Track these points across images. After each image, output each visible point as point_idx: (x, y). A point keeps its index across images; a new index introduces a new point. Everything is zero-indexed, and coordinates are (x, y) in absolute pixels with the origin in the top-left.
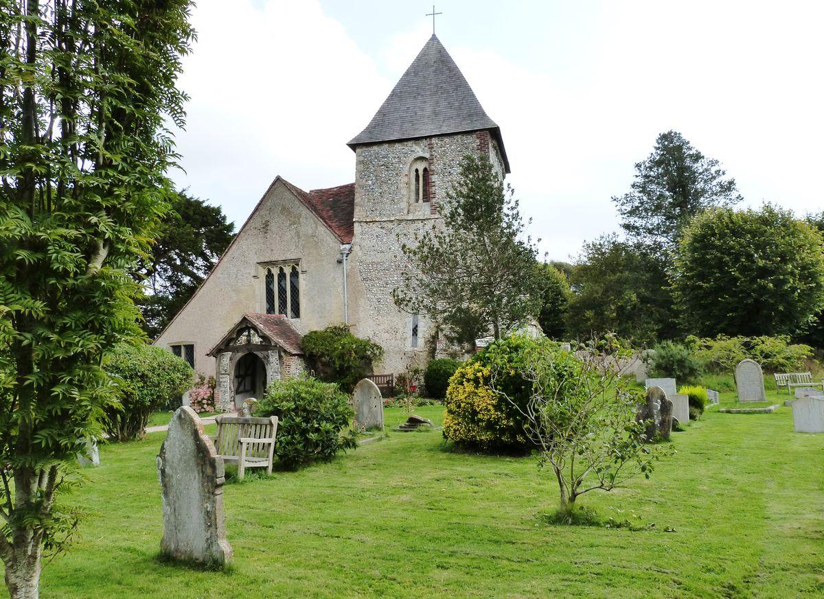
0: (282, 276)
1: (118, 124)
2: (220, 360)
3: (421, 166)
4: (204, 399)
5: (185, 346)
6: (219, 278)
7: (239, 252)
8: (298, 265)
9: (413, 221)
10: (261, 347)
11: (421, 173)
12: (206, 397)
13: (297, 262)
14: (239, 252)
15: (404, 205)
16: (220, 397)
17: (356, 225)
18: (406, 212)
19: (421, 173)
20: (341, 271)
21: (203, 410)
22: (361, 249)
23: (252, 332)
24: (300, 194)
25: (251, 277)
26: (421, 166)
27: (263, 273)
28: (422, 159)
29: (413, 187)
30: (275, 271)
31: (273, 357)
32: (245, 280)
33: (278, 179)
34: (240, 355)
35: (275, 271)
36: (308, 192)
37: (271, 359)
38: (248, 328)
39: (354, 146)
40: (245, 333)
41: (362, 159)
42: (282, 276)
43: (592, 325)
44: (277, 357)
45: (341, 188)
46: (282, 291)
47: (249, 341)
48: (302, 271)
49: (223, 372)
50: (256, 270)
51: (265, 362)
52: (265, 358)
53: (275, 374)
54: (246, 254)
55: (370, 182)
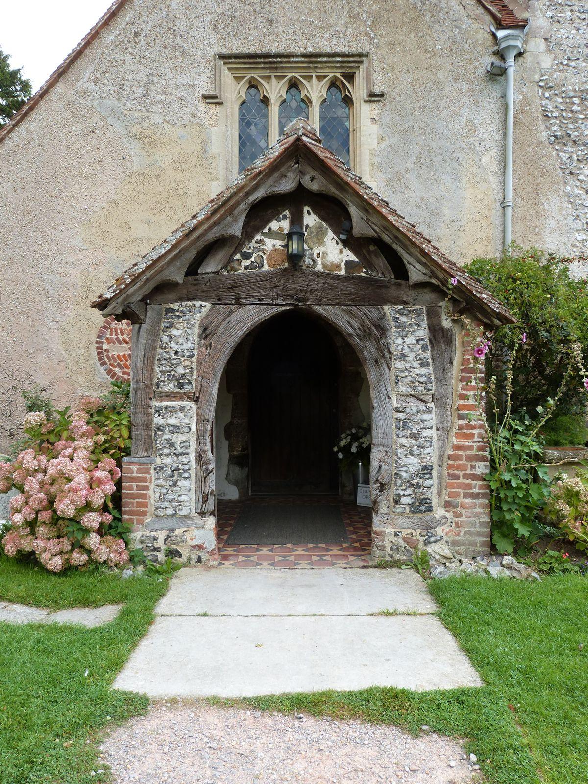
1: (128, 517)
2: (155, 334)
4: (88, 506)
6: (84, 94)
7: (157, 17)
8: (350, 77)
10: (351, 288)
12: (98, 500)
13: (344, 69)
14: (157, 17)
16: (153, 495)
20: (494, 106)
21: (79, 558)
22: (549, 50)
23: (310, 219)
32: (176, 106)
34: (250, 316)
35: (275, 90)
37: (396, 342)
40: (274, 225)
44: (423, 332)
48: (372, 95)
49: (171, 387)
50: (215, 78)
51: (368, 351)
52: (366, 334)
53: (414, 405)
54: (182, 25)
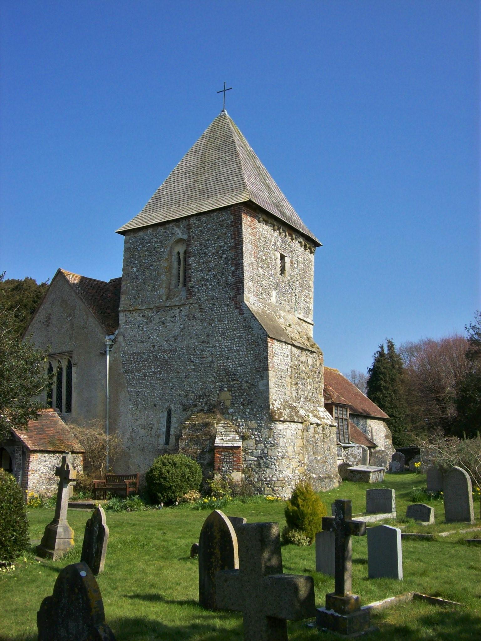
17: (121, 315)
28: (180, 241)
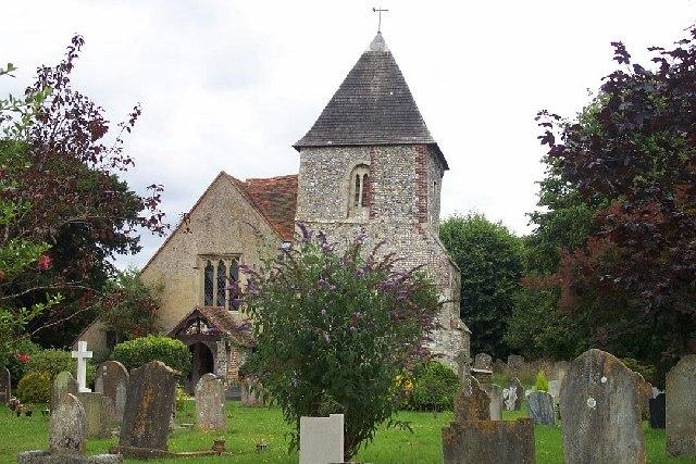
0: (221, 268)
3: (362, 172)
5: (662, 397)
9: (352, 225)
11: (361, 178)
15: (343, 209)
18: (345, 215)
19: (361, 178)
24: (238, 183)
25: (190, 268)
26: (362, 172)
27: (204, 264)
28: (362, 166)
29: (353, 192)
30: (215, 264)
31: (221, 347)
33: (222, 174)
35: (215, 264)
36: (244, 180)
38: (198, 320)
39: (298, 148)
41: (306, 160)
42: (221, 268)
43: (644, 177)
45: (278, 179)
46: (221, 284)
47: (199, 331)
55: (313, 184)
